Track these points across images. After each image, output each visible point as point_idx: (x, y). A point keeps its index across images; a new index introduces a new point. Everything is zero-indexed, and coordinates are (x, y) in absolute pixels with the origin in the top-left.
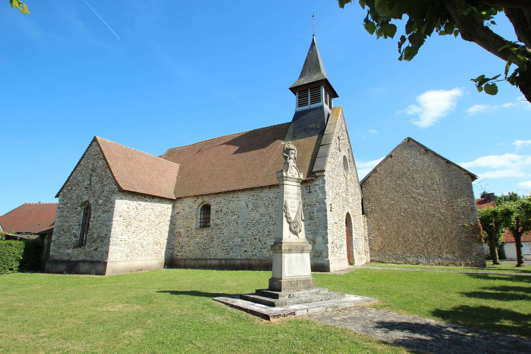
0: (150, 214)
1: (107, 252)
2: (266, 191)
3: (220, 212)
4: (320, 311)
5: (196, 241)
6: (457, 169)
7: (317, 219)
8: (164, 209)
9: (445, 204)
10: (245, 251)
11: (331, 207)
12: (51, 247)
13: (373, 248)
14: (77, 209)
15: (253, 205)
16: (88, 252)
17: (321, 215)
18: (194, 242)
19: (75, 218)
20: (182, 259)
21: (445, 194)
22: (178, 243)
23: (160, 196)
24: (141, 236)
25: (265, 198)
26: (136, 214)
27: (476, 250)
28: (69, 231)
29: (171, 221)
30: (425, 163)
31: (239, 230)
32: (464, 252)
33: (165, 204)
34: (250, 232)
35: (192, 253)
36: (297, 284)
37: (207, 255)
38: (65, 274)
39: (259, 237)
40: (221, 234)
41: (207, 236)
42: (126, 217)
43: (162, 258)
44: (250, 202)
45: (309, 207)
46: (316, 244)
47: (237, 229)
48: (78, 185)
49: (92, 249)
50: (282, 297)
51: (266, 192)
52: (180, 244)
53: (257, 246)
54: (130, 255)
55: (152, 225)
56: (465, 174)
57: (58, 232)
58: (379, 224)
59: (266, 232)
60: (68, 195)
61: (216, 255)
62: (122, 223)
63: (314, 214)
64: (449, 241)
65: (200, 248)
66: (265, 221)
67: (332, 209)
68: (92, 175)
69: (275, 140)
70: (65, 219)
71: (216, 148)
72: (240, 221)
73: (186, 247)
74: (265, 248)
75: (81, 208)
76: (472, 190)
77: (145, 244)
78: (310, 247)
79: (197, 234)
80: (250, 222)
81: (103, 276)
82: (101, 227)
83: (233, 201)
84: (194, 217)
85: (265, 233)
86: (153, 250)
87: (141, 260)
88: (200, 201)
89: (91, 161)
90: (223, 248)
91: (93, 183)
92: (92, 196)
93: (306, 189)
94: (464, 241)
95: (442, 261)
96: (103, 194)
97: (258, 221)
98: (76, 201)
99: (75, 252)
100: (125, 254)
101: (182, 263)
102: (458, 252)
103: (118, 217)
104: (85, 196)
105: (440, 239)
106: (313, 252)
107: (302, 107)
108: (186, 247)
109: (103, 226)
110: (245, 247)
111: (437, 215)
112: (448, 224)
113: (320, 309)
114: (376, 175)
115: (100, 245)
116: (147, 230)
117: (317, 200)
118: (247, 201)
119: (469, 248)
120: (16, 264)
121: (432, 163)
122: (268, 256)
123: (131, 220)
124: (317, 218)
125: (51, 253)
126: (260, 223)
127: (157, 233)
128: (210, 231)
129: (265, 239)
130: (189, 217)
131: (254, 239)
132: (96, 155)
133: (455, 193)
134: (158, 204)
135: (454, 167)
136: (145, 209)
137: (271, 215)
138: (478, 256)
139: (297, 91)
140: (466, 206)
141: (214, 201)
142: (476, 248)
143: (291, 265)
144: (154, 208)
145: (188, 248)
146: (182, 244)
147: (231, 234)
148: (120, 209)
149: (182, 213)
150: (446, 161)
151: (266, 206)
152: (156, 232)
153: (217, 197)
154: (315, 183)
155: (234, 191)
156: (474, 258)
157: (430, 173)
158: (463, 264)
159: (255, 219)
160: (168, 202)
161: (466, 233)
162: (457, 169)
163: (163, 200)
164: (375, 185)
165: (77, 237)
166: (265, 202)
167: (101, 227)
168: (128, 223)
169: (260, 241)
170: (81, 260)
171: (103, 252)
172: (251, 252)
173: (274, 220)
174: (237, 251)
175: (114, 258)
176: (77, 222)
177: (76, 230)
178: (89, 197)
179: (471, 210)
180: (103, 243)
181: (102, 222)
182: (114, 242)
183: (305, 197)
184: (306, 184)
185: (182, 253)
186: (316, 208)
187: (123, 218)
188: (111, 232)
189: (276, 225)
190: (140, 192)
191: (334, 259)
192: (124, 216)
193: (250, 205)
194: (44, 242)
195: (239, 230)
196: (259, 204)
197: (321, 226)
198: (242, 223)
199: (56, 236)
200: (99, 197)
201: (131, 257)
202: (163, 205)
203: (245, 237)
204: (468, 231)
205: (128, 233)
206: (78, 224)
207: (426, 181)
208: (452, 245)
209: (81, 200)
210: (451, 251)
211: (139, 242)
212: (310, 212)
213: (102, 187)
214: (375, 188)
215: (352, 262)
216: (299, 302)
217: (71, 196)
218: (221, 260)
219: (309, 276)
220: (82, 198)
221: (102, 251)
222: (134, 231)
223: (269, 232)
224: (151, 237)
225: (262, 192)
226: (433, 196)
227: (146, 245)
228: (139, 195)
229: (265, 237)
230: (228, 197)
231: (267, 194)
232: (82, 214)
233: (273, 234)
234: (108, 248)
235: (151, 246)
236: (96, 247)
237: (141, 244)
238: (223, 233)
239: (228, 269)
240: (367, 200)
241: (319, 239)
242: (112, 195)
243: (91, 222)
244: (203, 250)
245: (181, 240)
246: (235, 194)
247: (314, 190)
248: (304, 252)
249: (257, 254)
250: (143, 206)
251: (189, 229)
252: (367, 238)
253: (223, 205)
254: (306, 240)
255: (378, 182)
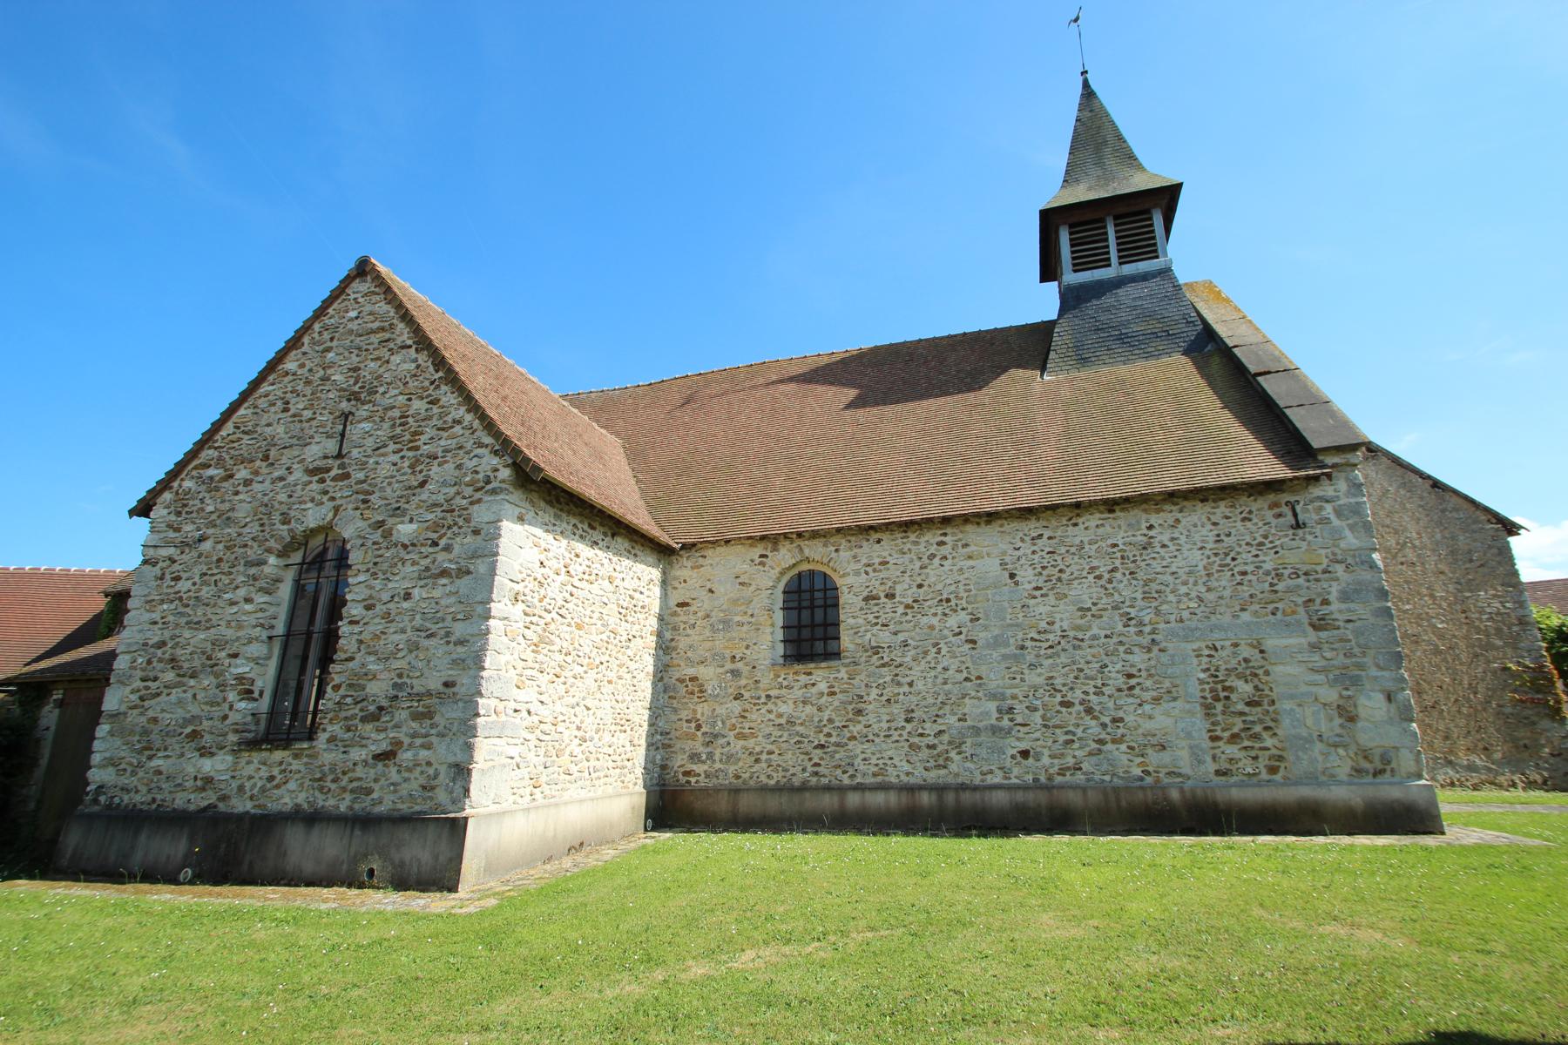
0: (606, 601)
1: (462, 772)
2: (1092, 520)
3: (883, 600)
5: (780, 716)
6: (1466, 505)
7: (1350, 626)
9: (1444, 605)
10: (1025, 754)
12: (97, 745)
15: (1040, 574)
16: (333, 770)
18: (772, 716)
19: (248, 607)
20: (717, 790)
21: (1442, 577)
22: (688, 721)
27: (1549, 741)
28: (212, 665)
29: (659, 635)
30: (1372, 484)
31: (983, 670)
32: (1517, 747)
34: (1040, 675)
35: (764, 765)
37: (839, 772)
38: (191, 882)
40: (899, 684)
41: (833, 693)
42: (536, 601)
44: (1023, 561)
45: (1301, 581)
46: (1360, 724)
47: (974, 663)
48: (266, 458)
49: (357, 754)
52: (699, 727)
55: (610, 646)
56: (1489, 521)
57: (139, 674)
59: (1113, 675)
60: (207, 501)
61: (882, 772)
64: (1469, 715)
65: (799, 742)
68: (351, 413)
70: (188, 610)
72: (982, 637)
73: (731, 738)
75: (282, 562)
76: (1513, 565)
79: (781, 687)
81: (435, 903)
82: (414, 647)
83: (945, 558)
84: (761, 619)
85: (1110, 682)
87: (581, 801)
88: (785, 556)
89: (345, 359)
90: (916, 740)
91: (355, 452)
92: (351, 506)
94: (1512, 714)
95: (1458, 776)
96: (424, 497)
98: (254, 528)
99: (249, 771)
100: (527, 777)
101: (722, 805)
102: (1499, 748)
103: (506, 600)
104: (310, 505)
105: (1443, 707)
107: (1089, 272)
108: (731, 738)
109: (425, 643)
110: (1021, 735)
111: (1425, 638)
112: (1461, 664)
115: (414, 735)
118: (1008, 559)
119: (1529, 734)
121: (1391, 485)
123: (548, 617)
124: (1349, 621)
125: (96, 776)
128: (843, 674)
130: (737, 618)
131: (1062, 704)
132: (373, 332)
133: (1468, 574)
135: (1455, 499)
137: (1129, 610)
138: (1558, 759)
139: (1065, 223)
140: (1503, 611)
141: (855, 557)
142: (1549, 734)
145: (742, 743)
146: (714, 725)
147: (945, 683)
149: (704, 603)
150: (1431, 482)
151: (1099, 577)
153: (865, 544)
155: (946, 521)
156: (1546, 765)
157: (1389, 514)
158: (1520, 785)
159: (1057, 626)
161: (1515, 691)
162: (1465, 507)
165: (256, 695)
166: (1095, 563)
167: (414, 647)
168: (539, 629)
170: (289, 808)
171: (431, 771)
174: (983, 752)
175: (492, 796)
176: (262, 625)
177: (256, 661)
178: (336, 510)
179: (1521, 624)
180: (432, 726)
181: (418, 621)
183: (1277, 543)
184: (1272, 497)
185: (714, 762)
186: (1334, 584)
188: (483, 668)
192: (529, 598)
193: (1027, 576)
194: (36, 720)
197: (1372, 652)
198: (997, 642)
199: (128, 689)
200: (397, 512)
203: (1014, 697)
204: (1520, 686)
205: (539, 675)
206: (265, 634)
207: (1383, 537)
208: (1480, 727)
209: (286, 522)
210: (1480, 746)
211: (573, 719)
213: (412, 467)
217: (227, 506)
218: (911, 789)
220: (292, 513)
221: (429, 764)
223: (1130, 676)
224: (606, 697)
225: (1075, 525)
226: (1407, 582)
230: (916, 543)
231: (1101, 531)
232: (285, 591)
233: (1149, 683)
234: (469, 748)
235: (607, 737)
236: (384, 746)
237: (579, 728)
238: (908, 680)
242: (479, 501)
243: (351, 623)
244: (818, 751)
245: (703, 710)
246: (949, 530)
247: (1315, 517)
249: (1085, 766)
251: (740, 665)
253: (898, 573)
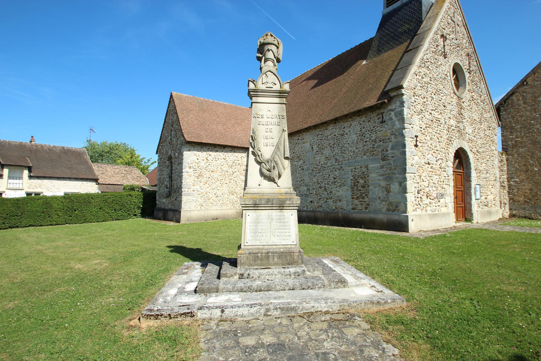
2: (331, 127)
4: (252, 314)
7: (393, 159)
8: (238, 158)
10: (311, 202)
11: (417, 141)
13: (516, 198)
14: (166, 163)
15: (318, 147)
17: (397, 152)
23: (230, 145)
24: (214, 186)
25: (330, 136)
26: (207, 165)
33: (239, 154)
36: (268, 257)
39: (324, 185)
42: (197, 167)
43: (239, 208)
45: (381, 143)
50: (226, 277)
51: (330, 128)
53: (323, 195)
54: (204, 204)
55: (225, 175)
58: (528, 164)
59: (331, 178)
62: (193, 174)
63: (388, 153)
66: (330, 165)
67: (418, 143)
69: (356, 61)
71: (297, 87)
74: (331, 198)
77: (220, 194)
78: (297, 200)
80: (315, 168)
83: (299, 144)
85: (331, 181)
86: (229, 199)
93: (379, 118)
97: (323, 166)
103: (187, 168)
106: (387, 204)
110: (311, 196)
113: (252, 310)
114: (526, 89)
116: (221, 180)
117: (393, 132)
120: (139, 211)
122: (334, 208)
123: (202, 171)
124: (392, 157)
126: (325, 168)
127: (232, 183)
129: (330, 188)
134: (230, 154)
136: (216, 159)
143: (259, 228)
144: (226, 157)
147: (297, 182)
148: (189, 161)
152: (230, 182)
154: (390, 107)
160: (242, 151)
163: (236, 149)
164: (523, 105)
168: (199, 174)
169: (325, 189)
172: (317, 203)
173: (340, 163)
175: (188, 207)
182: (187, 192)
186: (391, 143)
187: (193, 169)
189: (343, 170)
190: (206, 142)
191: (420, 215)
192: (194, 167)
193: (315, 147)
195: (305, 177)
196: (324, 145)
198: (308, 169)
201: (206, 207)
202: (236, 154)
203: (310, 186)
211: (213, 192)
212: (383, 150)
214: (523, 110)
215: (468, 217)
216: (245, 289)
219: (293, 246)
222: (206, 182)
223: (335, 179)
225: (327, 129)
227: (221, 195)
228: (208, 146)
229: (330, 185)
233: (339, 181)
235: (226, 196)
239: (309, 223)
240: (507, 129)
241: (395, 187)
246: (300, 135)
247: (388, 118)
248: (285, 208)
250: (214, 156)
252: (506, 184)
254: (292, 189)
255: (528, 101)
